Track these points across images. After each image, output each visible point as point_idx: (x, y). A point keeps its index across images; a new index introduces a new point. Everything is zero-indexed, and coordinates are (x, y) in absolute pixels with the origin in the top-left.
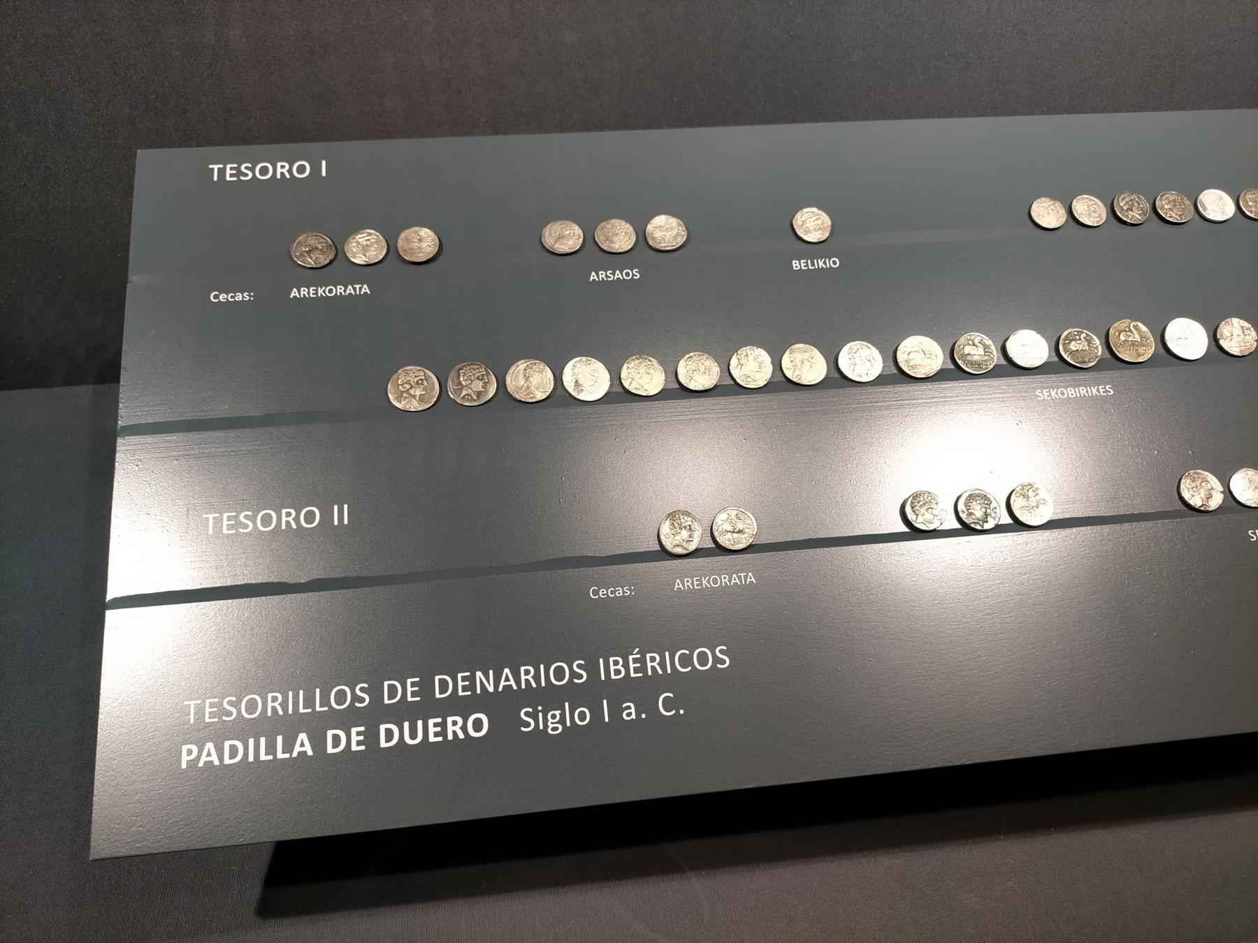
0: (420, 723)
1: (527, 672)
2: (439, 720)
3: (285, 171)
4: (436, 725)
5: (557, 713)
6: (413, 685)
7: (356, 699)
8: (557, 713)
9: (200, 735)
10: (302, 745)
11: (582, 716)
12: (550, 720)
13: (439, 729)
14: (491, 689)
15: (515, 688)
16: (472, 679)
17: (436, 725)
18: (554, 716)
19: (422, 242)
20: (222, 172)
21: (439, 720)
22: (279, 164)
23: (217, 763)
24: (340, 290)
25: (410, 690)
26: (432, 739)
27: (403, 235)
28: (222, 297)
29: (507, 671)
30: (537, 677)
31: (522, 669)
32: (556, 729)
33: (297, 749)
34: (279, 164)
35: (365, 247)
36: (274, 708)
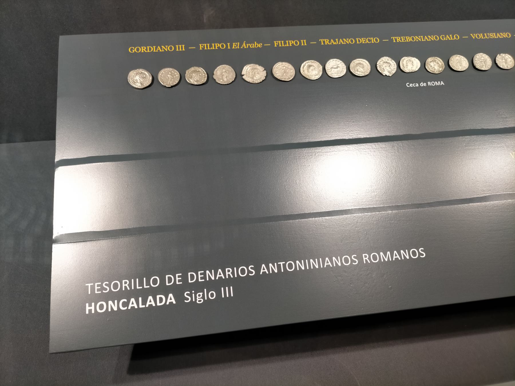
1: (366, 256)
5: (201, 294)
6: (179, 277)
7: (249, 272)
8: (201, 294)
9: (95, 299)
10: (133, 303)
11: (212, 295)
12: (198, 297)
14: (213, 278)
15: (224, 278)
16: (205, 274)
20: (93, 288)
25: (177, 279)
28: (411, 85)
30: (233, 273)
31: (227, 269)
33: (148, 303)
36: (125, 287)
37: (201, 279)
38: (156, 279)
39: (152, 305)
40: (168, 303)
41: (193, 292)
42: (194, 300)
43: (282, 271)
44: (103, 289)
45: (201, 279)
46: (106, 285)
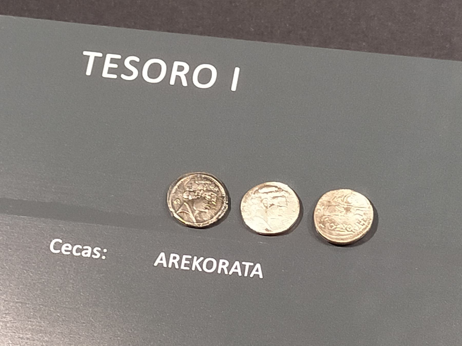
2: (190, 257)
3: (182, 75)
4: (187, 259)
10: (236, 268)
13: (188, 262)
19: (348, 213)
20: (99, 63)
21: (190, 257)
22: (172, 255)
24: (223, 265)
27: (325, 198)
34: (172, 255)
35: (269, 209)
36: (178, 78)
37: (109, 73)
38: (209, 71)
39: (162, 264)
40: (252, 275)
43: (89, 73)
45: (109, 73)
46: (132, 63)
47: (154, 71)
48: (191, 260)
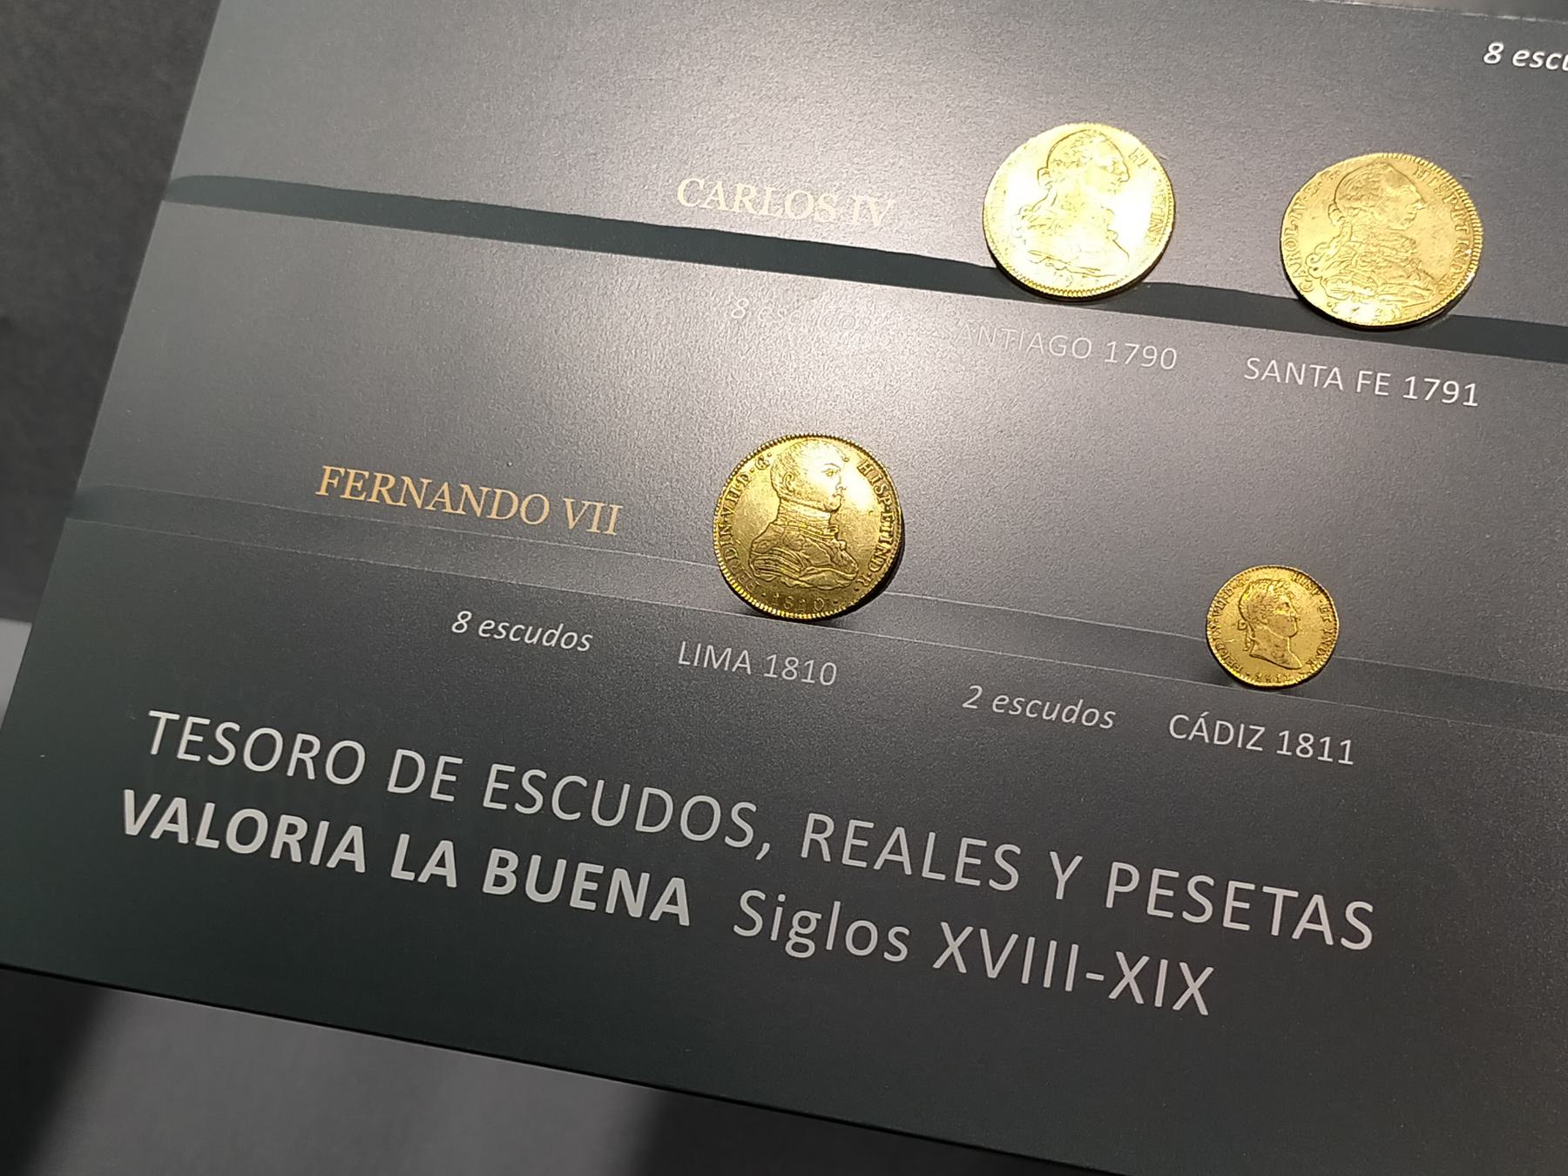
0: (561, 864)
2: (599, 869)
4: (590, 877)
6: (448, 768)
8: (814, 917)
12: (796, 927)
13: (593, 886)
15: (908, 871)
17: (590, 877)
18: (805, 922)
20: (174, 730)
21: (599, 869)
23: (183, 839)
26: (576, 902)
29: (900, 831)
32: (805, 948)
33: (431, 869)
39: (175, 834)
40: (655, 916)
41: (782, 898)
42: (774, 937)
44: (1182, 902)
47: (263, 750)
48: (604, 881)
